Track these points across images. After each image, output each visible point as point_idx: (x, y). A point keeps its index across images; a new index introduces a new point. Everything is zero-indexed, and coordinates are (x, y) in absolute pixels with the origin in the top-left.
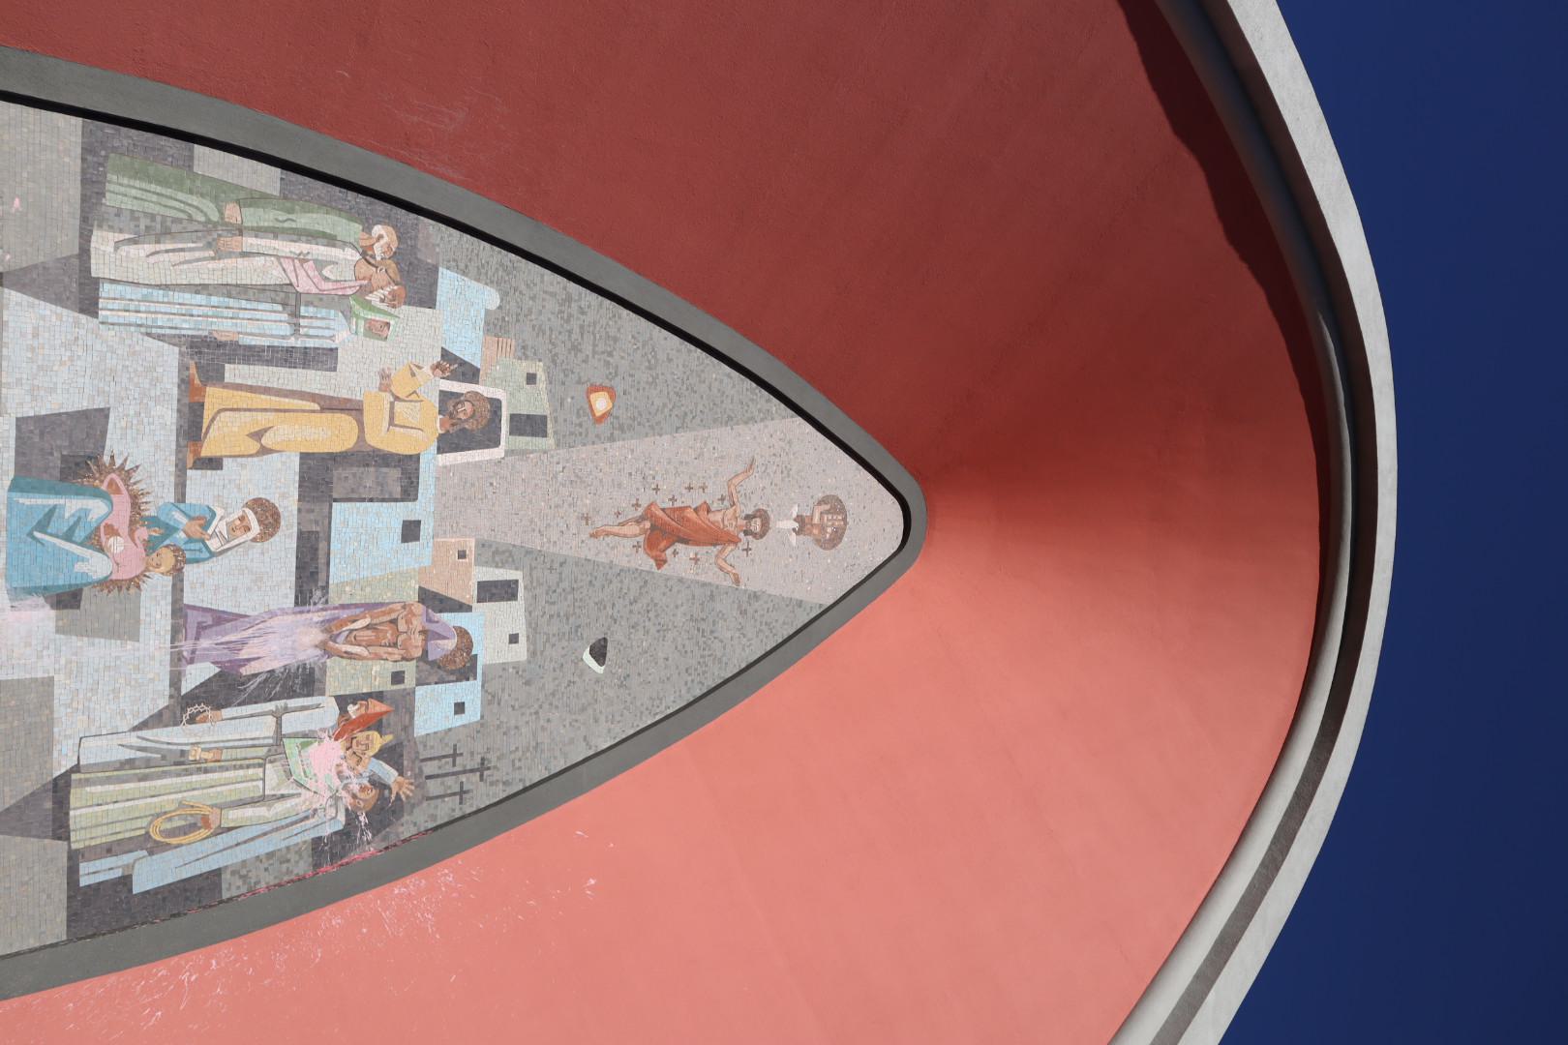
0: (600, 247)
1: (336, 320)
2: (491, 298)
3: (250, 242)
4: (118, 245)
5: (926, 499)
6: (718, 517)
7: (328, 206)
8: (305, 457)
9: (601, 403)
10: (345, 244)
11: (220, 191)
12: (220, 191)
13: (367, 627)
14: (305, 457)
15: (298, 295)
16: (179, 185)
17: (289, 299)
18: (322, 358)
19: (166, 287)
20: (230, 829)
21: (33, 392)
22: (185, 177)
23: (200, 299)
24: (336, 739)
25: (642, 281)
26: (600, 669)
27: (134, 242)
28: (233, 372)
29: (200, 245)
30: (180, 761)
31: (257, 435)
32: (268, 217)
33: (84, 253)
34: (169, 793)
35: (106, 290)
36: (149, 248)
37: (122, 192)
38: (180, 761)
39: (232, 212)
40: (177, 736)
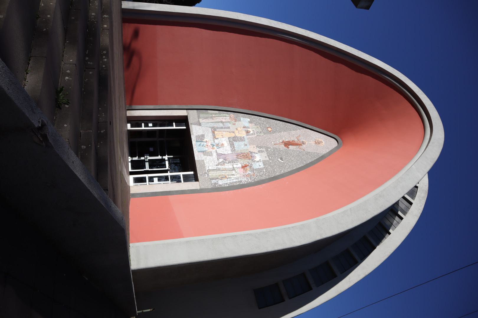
0: (280, 116)
1: (228, 124)
2: (249, 120)
3: (216, 118)
4: (202, 120)
5: (340, 138)
6: (297, 142)
7: (224, 113)
8: (187, 116)
9: (270, 129)
10: (227, 117)
11: (212, 114)
12: (212, 114)
13: (242, 155)
14: (187, 116)
15: (223, 122)
16: (207, 114)
17: (222, 122)
18: (229, 128)
19: (208, 123)
20: (202, 151)
21: (196, 133)
22: (208, 113)
23: (212, 123)
24: (242, 168)
25: (277, 116)
26: (283, 162)
27: (203, 119)
28: (217, 130)
29: (30, 54)
30: (219, 170)
31: (222, 136)
32: (217, 115)
33: (199, 121)
34: (218, 173)
35: (202, 124)
36: (205, 120)
37: (201, 115)
38: (219, 170)
39: (214, 115)
40: (219, 167)
